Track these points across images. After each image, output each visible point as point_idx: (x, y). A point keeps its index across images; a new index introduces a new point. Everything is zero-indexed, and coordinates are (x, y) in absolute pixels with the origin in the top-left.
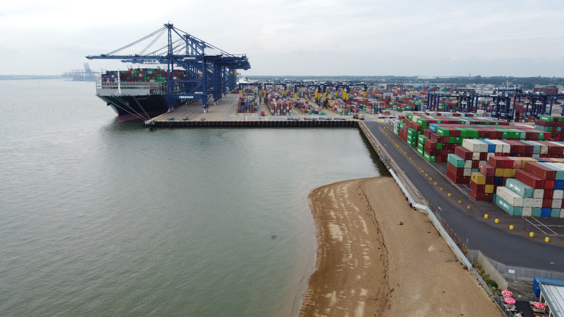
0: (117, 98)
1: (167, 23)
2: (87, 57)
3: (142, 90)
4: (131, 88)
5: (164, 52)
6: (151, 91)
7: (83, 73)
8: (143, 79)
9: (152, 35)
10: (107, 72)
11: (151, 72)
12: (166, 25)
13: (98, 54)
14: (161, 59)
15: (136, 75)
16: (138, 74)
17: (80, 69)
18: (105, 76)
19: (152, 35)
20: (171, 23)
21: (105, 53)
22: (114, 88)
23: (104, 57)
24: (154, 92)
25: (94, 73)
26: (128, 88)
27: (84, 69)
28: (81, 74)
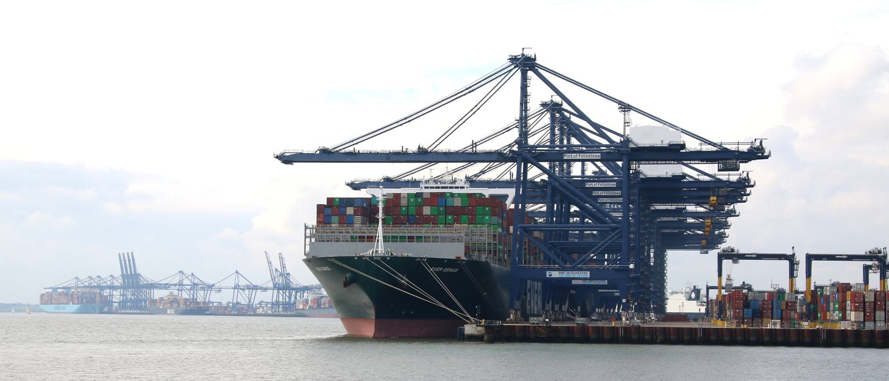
0: (377, 262)
1: (518, 53)
2: (286, 159)
3: (446, 246)
4: (411, 239)
5: (508, 140)
6: (467, 250)
7: (112, 287)
8: (432, 220)
9: (470, 89)
10: (329, 200)
11: (458, 203)
12: (513, 59)
13: (311, 148)
14: (498, 157)
15: (413, 211)
16: (419, 208)
17: (105, 275)
18: (328, 211)
19: (470, 89)
20: (529, 53)
21: (330, 145)
22: (362, 239)
23: (326, 155)
24: (475, 256)
25: (152, 286)
26: (402, 239)
27: (118, 273)
28: (106, 292)
